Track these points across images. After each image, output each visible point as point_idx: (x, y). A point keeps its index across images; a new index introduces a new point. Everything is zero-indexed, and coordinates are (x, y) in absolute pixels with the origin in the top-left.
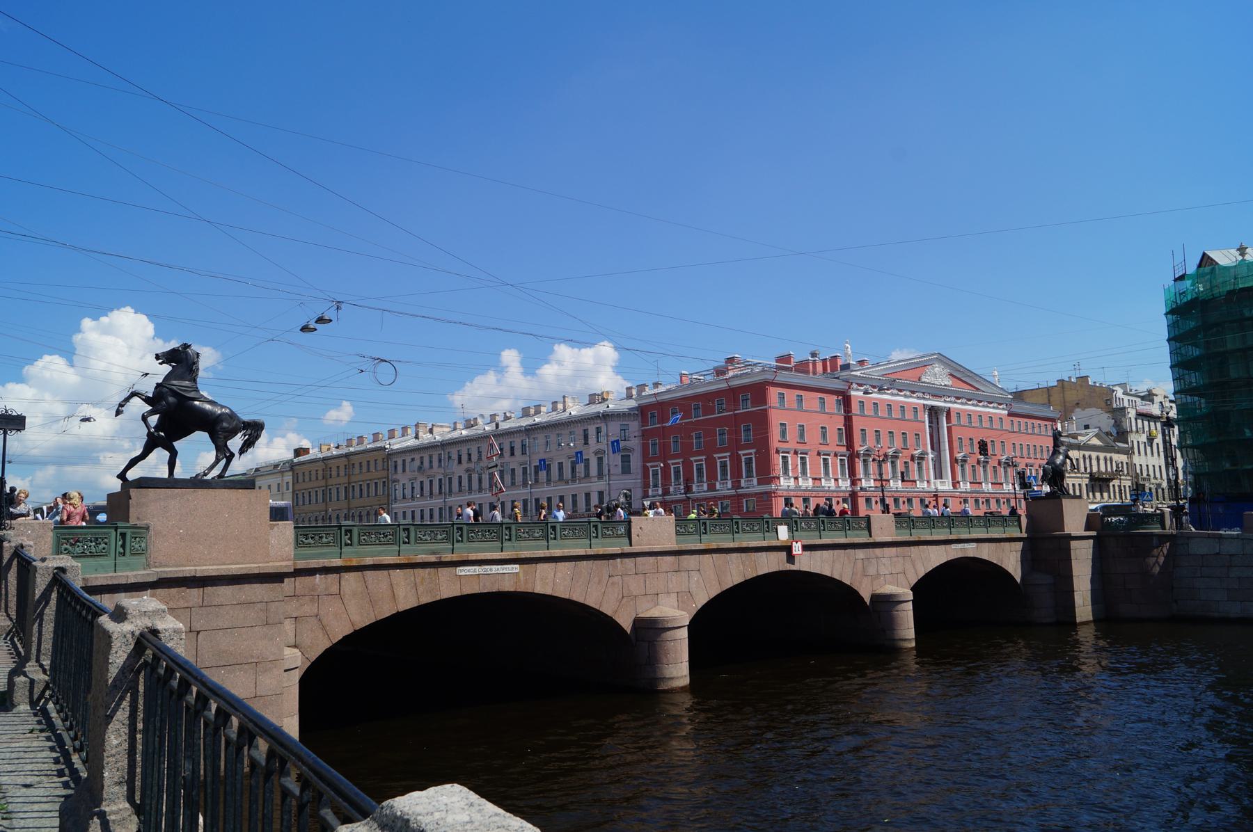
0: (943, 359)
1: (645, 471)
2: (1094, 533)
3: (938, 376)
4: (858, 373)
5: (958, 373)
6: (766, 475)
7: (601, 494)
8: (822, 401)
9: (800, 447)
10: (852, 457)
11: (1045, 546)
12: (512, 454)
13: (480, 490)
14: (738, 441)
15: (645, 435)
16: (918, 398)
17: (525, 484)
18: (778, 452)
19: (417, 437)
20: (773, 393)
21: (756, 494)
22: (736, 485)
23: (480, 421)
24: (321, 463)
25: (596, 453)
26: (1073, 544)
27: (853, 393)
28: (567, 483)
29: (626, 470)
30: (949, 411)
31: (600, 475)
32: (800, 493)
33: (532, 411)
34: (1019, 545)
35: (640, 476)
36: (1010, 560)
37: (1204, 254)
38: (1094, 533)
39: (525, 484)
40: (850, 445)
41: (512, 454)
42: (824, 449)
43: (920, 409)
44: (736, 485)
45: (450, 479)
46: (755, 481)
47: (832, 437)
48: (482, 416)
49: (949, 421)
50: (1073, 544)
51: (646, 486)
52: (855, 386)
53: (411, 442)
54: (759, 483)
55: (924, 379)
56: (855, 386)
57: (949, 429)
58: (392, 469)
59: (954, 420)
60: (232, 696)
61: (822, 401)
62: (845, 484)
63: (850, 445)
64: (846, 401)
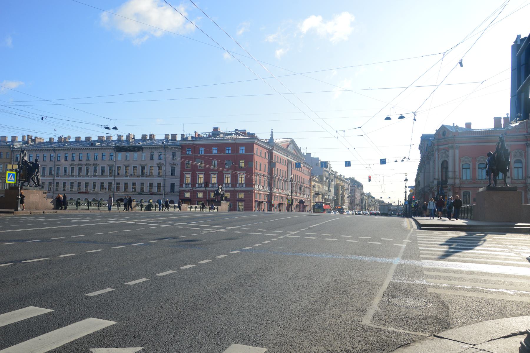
7: (159, 185)
27: (274, 151)
39: (87, 175)
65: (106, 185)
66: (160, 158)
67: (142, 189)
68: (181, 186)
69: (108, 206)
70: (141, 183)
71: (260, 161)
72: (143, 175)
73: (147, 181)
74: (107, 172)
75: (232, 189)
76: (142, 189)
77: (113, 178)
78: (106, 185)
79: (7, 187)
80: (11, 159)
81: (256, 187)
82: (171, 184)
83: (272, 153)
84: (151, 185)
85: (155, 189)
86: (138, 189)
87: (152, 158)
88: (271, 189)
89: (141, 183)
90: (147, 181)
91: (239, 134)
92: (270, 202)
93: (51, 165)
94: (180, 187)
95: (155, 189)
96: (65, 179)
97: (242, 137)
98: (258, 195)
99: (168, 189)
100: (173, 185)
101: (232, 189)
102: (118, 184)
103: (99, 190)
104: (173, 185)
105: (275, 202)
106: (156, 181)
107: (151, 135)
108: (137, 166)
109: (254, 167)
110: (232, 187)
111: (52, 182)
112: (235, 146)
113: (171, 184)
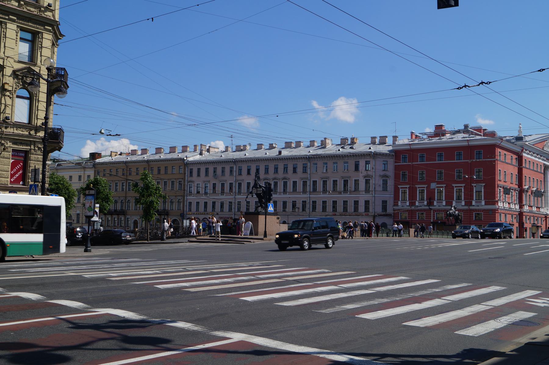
1: (396, 190)
6: (491, 198)
7: (367, 203)
10: (521, 192)
12: (199, 175)
13: (223, 192)
15: (397, 168)
17: (304, 192)
19: (201, 154)
21: (484, 210)
22: (412, 204)
23: (248, 147)
24: (145, 163)
25: (365, 177)
27: (524, 155)
28: (340, 193)
29: (385, 189)
31: (367, 190)
32: (510, 212)
33: (293, 145)
35: (393, 193)
37: (386, 137)
39: (285, 191)
40: (520, 184)
41: (199, 175)
44: (412, 204)
45: (240, 185)
46: (483, 203)
47: (514, 177)
48: (250, 144)
51: (396, 198)
53: (197, 157)
54: (486, 204)
58: (187, 173)
62: (517, 207)
63: (520, 184)
64: (520, 159)
65: (299, 205)
66: (305, 171)
67: (345, 209)
68: (396, 204)
69: (116, 211)
70: (303, 201)
71: (505, 170)
72: (345, 190)
73: (350, 197)
74: (340, 186)
75: (466, 207)
76: (345, 209)
77: (307, 195)
78: (299, 205)
79: (413, 226)
80: (185, 174)
81: (500, 204)
82: (365, 201)
83: (522, 156)
84: (356, 203)
85: (362, 209)
86: (340, 208)
87: (357, 168)
88: (521, 207)
89: (303, 201)
90: (350, 197)
91: (472, 133)
92: (521, 224)
93: (231, 180)
94: (394, 205)
95: (362, 209)
96: (335, 197)
97: (478, 137)
98: (503, 215)
99: (379, 210)
100: (384, 203)
101: (466, 207)
102: (314, 202)
103: (291, 210)
104: (384, 203)
105: (528, 225)
106: (362, 198)
107: (353, 139)
108: (297, 180)
109: (497, 177)
110: (466, 205)
111: (233, 201)
112: (468, 150)
113: (365, 201)
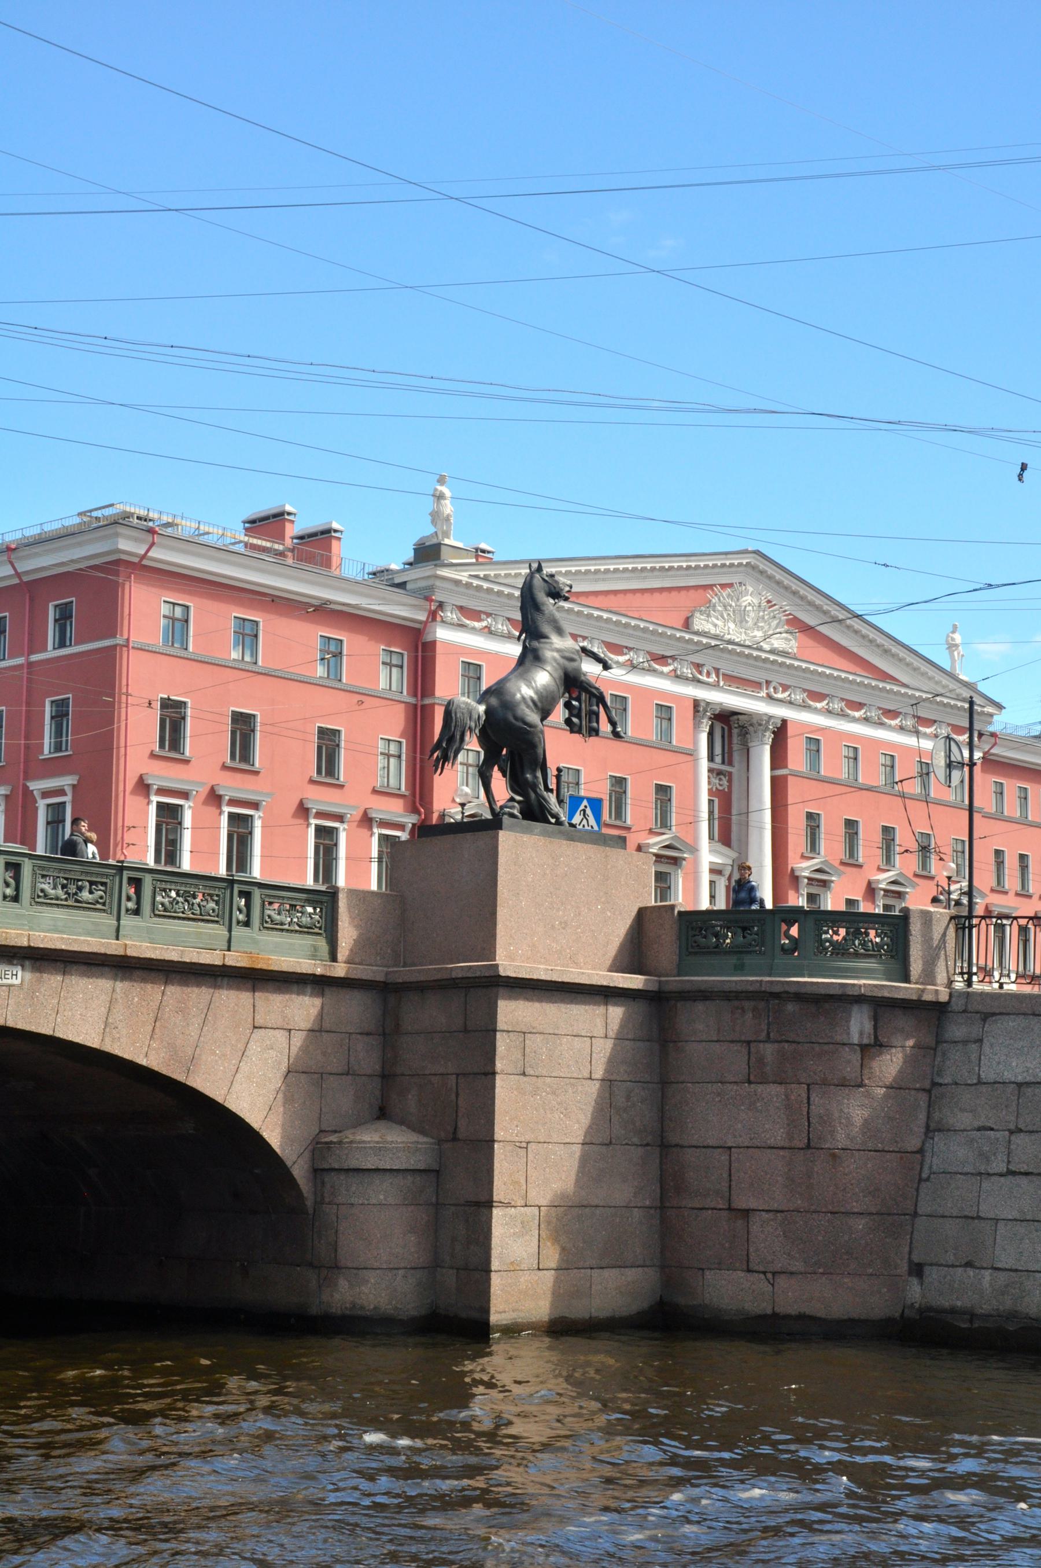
0: (763, 569)
2: (635, 981)
3: (746, 621)
4: (463, 576)
5: (819, 619)
8: (333, 654)
9: (232, 786)
11: (420, 1012)
14: (32, 750)
16: (677, 677)
18: (143, 787)
20: (146, 611)
26: (511, 1012)
27: (442, 634)
30: (781, 732)
34: (303, 1009)
36: (249, 1066)
38: (635, 981)
42: (321, 798)
43: (682, 719)
49: (778, 758)
50: (511, 1012)
52: (451, 615)
55: (700, 623)
56: (451, 615)
57: (778, 786)
59: (797, 758)
60: (603, 1314)
61: (333, 654)
